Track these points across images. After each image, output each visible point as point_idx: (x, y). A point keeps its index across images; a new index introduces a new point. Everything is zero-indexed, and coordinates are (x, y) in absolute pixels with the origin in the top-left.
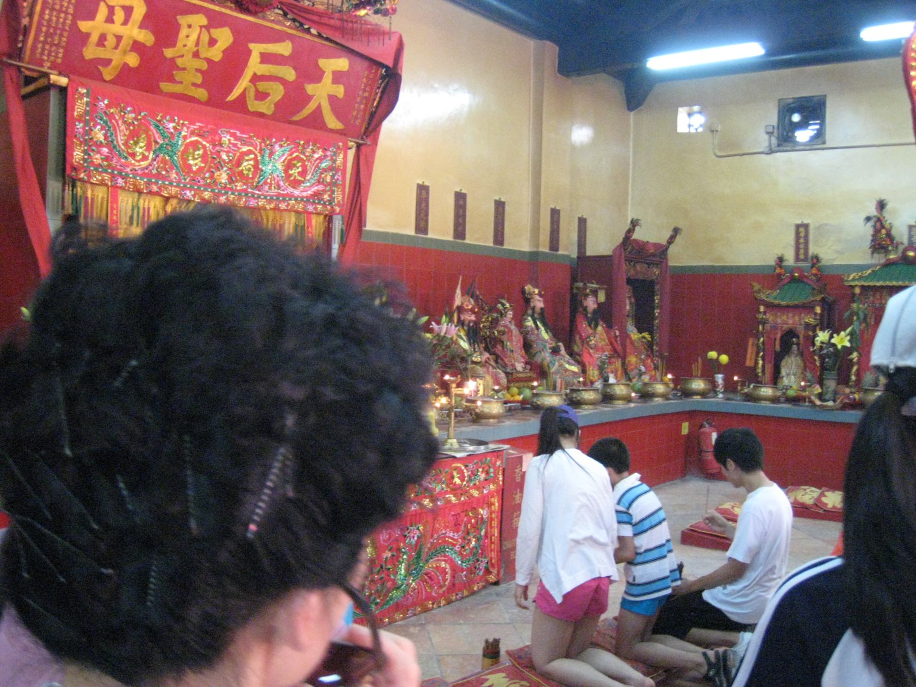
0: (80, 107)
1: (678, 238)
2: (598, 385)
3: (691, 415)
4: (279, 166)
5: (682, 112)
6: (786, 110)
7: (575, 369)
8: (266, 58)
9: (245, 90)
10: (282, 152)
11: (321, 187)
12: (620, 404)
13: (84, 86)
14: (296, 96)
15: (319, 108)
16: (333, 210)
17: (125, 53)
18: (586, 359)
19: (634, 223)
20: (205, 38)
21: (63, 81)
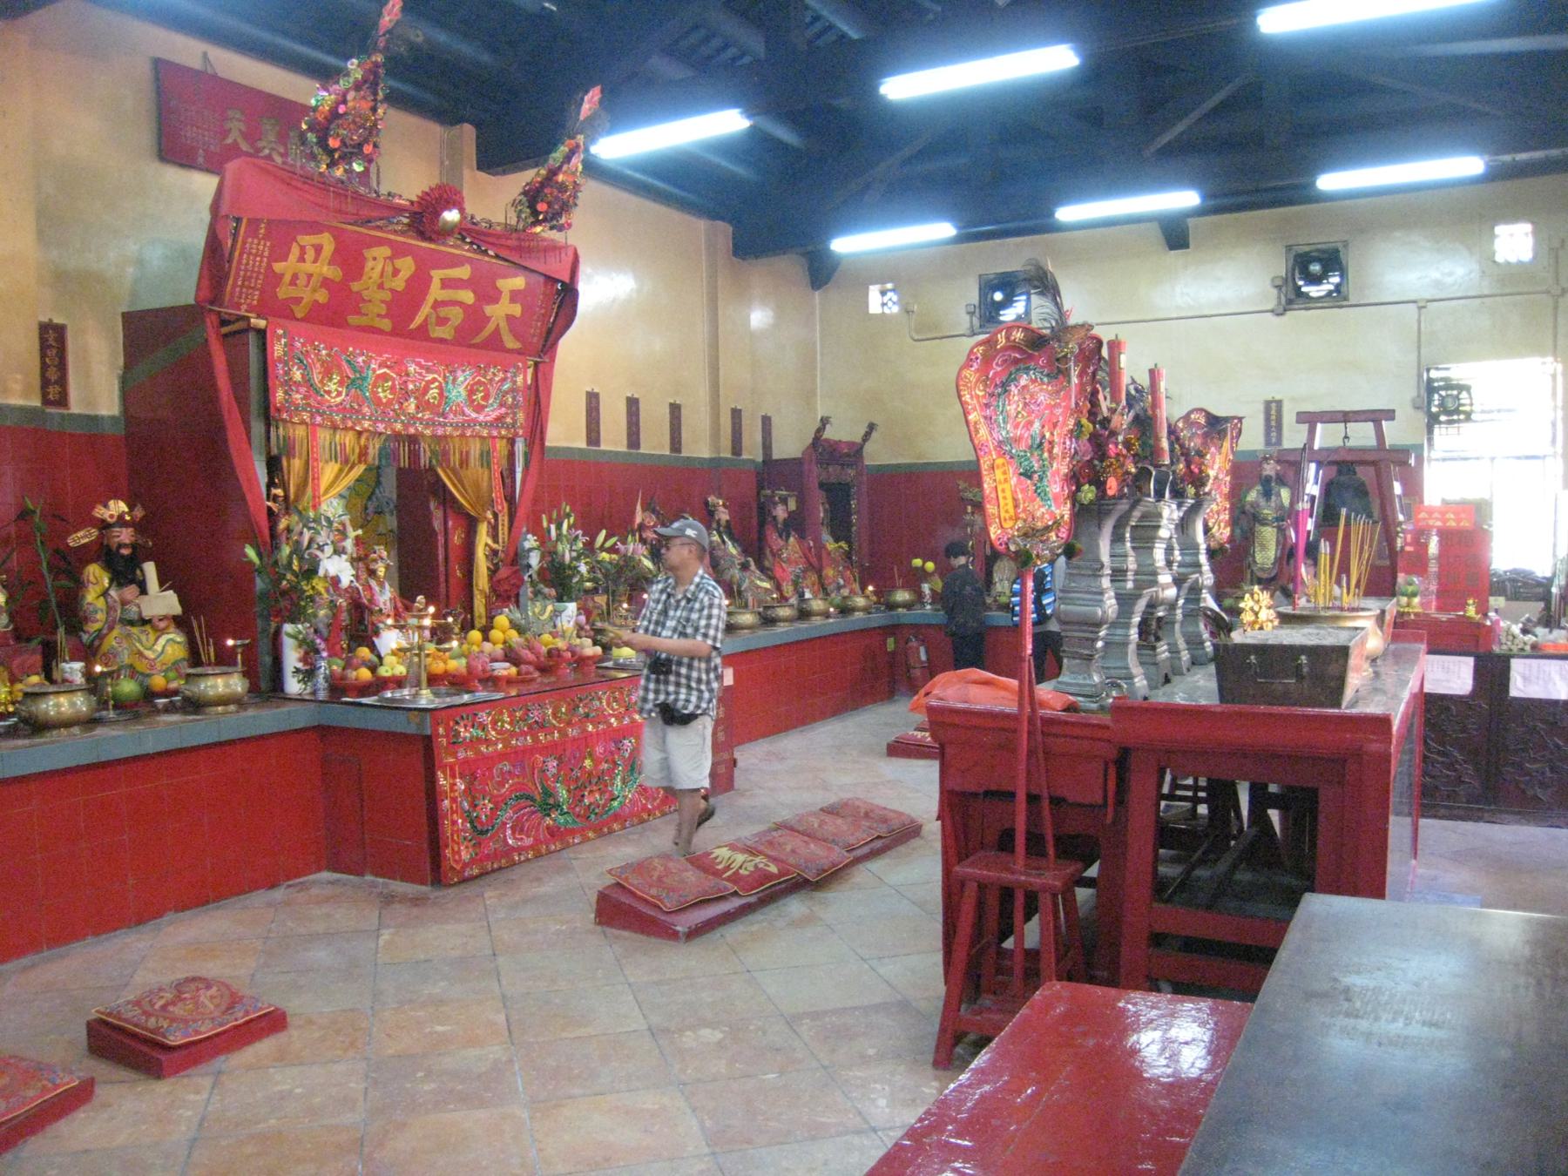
0: (278, 349)
1: (874, 434)
2: (793, 601)
3: (893, 629)
4: (464, 393)
5: (874, 291)
6: (987, 287)
7: (766, 585)
8: (447, 284)
9: (426, 320)
10: (464, 377)
11: (503, 410)
12: (817, 621)
13: (281, 327)
14: (475, 319)
15: (497, 331)
16: (516, 435)
17: (314, 291)
18: (778, 573)
19: (825, 421)
20: (389, 269)
21: (262, 323)
